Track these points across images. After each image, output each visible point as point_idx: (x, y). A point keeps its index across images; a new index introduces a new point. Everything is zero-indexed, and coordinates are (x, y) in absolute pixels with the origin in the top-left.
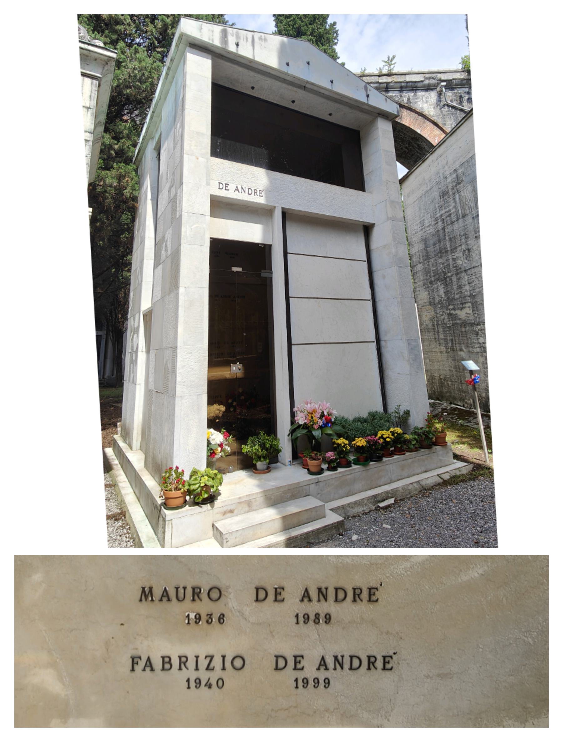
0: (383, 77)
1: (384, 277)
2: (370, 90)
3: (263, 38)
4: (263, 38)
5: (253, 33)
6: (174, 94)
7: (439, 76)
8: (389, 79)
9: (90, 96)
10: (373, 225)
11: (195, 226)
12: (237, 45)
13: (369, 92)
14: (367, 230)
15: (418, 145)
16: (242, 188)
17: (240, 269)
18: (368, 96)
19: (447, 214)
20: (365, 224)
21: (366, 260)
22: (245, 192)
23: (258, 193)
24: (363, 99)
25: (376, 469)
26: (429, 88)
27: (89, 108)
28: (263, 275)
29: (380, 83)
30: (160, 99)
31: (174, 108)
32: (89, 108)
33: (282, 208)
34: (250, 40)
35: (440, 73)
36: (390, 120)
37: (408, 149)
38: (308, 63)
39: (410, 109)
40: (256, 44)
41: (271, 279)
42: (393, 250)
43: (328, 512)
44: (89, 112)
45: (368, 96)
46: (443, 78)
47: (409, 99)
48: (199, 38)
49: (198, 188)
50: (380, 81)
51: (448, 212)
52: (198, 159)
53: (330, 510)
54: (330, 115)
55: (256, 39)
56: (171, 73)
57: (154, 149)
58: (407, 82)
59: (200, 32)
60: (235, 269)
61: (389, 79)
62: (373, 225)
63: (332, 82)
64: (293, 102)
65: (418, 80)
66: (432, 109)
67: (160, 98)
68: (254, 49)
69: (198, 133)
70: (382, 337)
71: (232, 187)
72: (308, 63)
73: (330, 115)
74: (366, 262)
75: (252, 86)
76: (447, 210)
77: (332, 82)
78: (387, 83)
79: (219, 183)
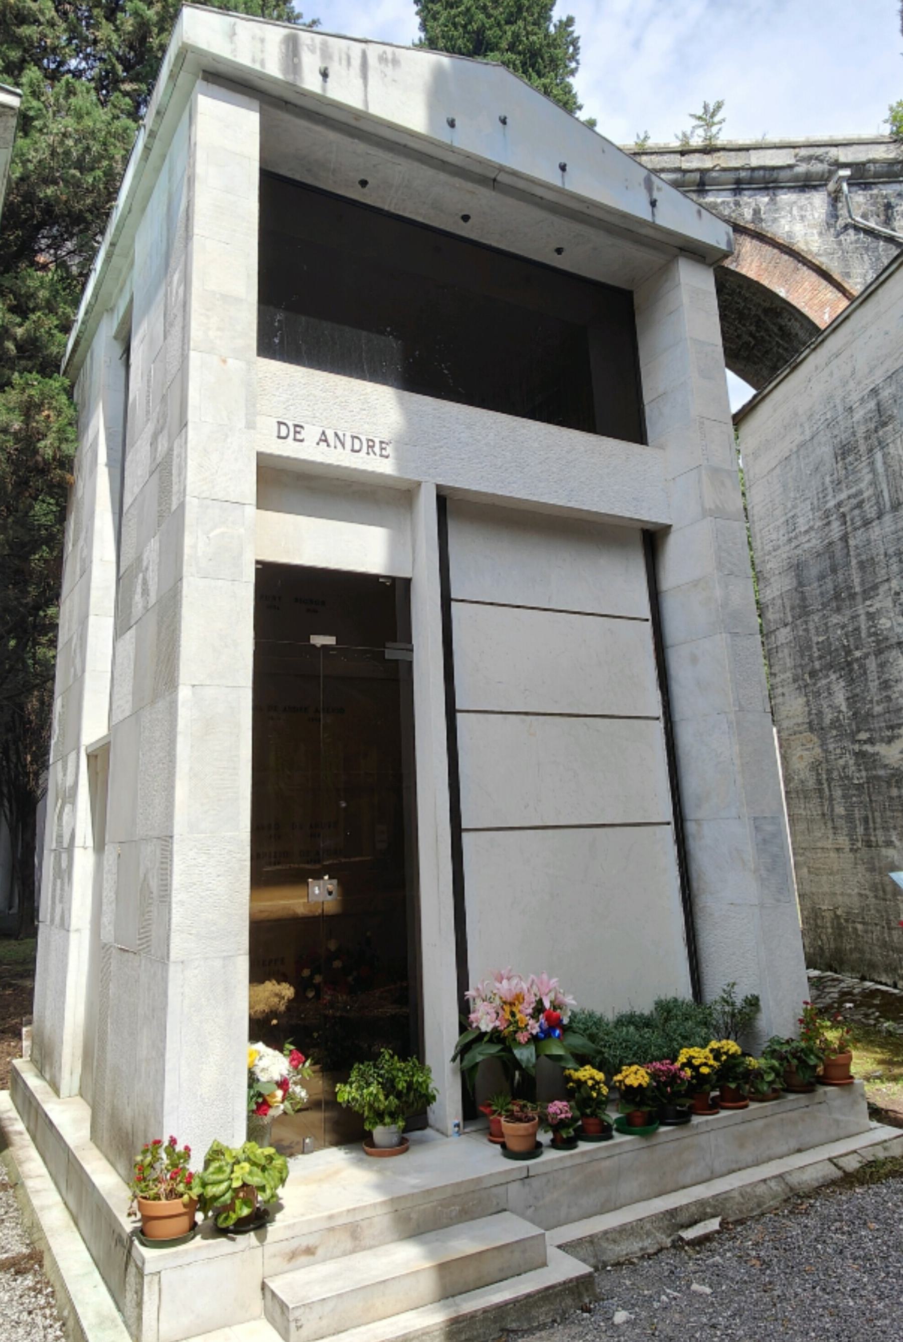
1: (694, 660)
2: (659, 189)
3: (390, 57)
4: (390, 57)
5: (363, 45)
6: (165, 199)
7: (833, 152)
10: (666, 529)
12: (325, 74)
13: (656, 195)
14: (652, 541)
15: (781, 328)
16: (336, 435)
18: (653, 204)
19: (854, 501)
21: (649, 617)
22: (343, 445)
23: (377, 449)
24: (642, 211)
26: (806, 184)
28: (389, 655)
29: (685, 172)
30: (129, 212)
33: (438, 487)
34: (356, 62)
35: (836, 146)
36: (710, 265)
38: (504, 121)
39: (760, 237)
40: (371, 74)
41: (410, 664)
42: (718, 593)
45: (653, 204)
46: (842, 159)
47: (756, 212)
48: (229, 56)
49: (227, 436)
50: (685, 166)
51: (855, 496)
52: (224, 361)
53: (559, 1247)
54: (559, 251)
59: (232, 42)
60: (318, 640)
61: (707, 162)
62: (666, 529)
63: (563, 168)
64: (466, 218)
70: (691, 812)
71: (311, 433)
72: (504, 121)
73: (559, 251)
74: (650, 623)
75: (362, 177)
77: (563, 168)
78: (703, 171)
79: (280, 423)
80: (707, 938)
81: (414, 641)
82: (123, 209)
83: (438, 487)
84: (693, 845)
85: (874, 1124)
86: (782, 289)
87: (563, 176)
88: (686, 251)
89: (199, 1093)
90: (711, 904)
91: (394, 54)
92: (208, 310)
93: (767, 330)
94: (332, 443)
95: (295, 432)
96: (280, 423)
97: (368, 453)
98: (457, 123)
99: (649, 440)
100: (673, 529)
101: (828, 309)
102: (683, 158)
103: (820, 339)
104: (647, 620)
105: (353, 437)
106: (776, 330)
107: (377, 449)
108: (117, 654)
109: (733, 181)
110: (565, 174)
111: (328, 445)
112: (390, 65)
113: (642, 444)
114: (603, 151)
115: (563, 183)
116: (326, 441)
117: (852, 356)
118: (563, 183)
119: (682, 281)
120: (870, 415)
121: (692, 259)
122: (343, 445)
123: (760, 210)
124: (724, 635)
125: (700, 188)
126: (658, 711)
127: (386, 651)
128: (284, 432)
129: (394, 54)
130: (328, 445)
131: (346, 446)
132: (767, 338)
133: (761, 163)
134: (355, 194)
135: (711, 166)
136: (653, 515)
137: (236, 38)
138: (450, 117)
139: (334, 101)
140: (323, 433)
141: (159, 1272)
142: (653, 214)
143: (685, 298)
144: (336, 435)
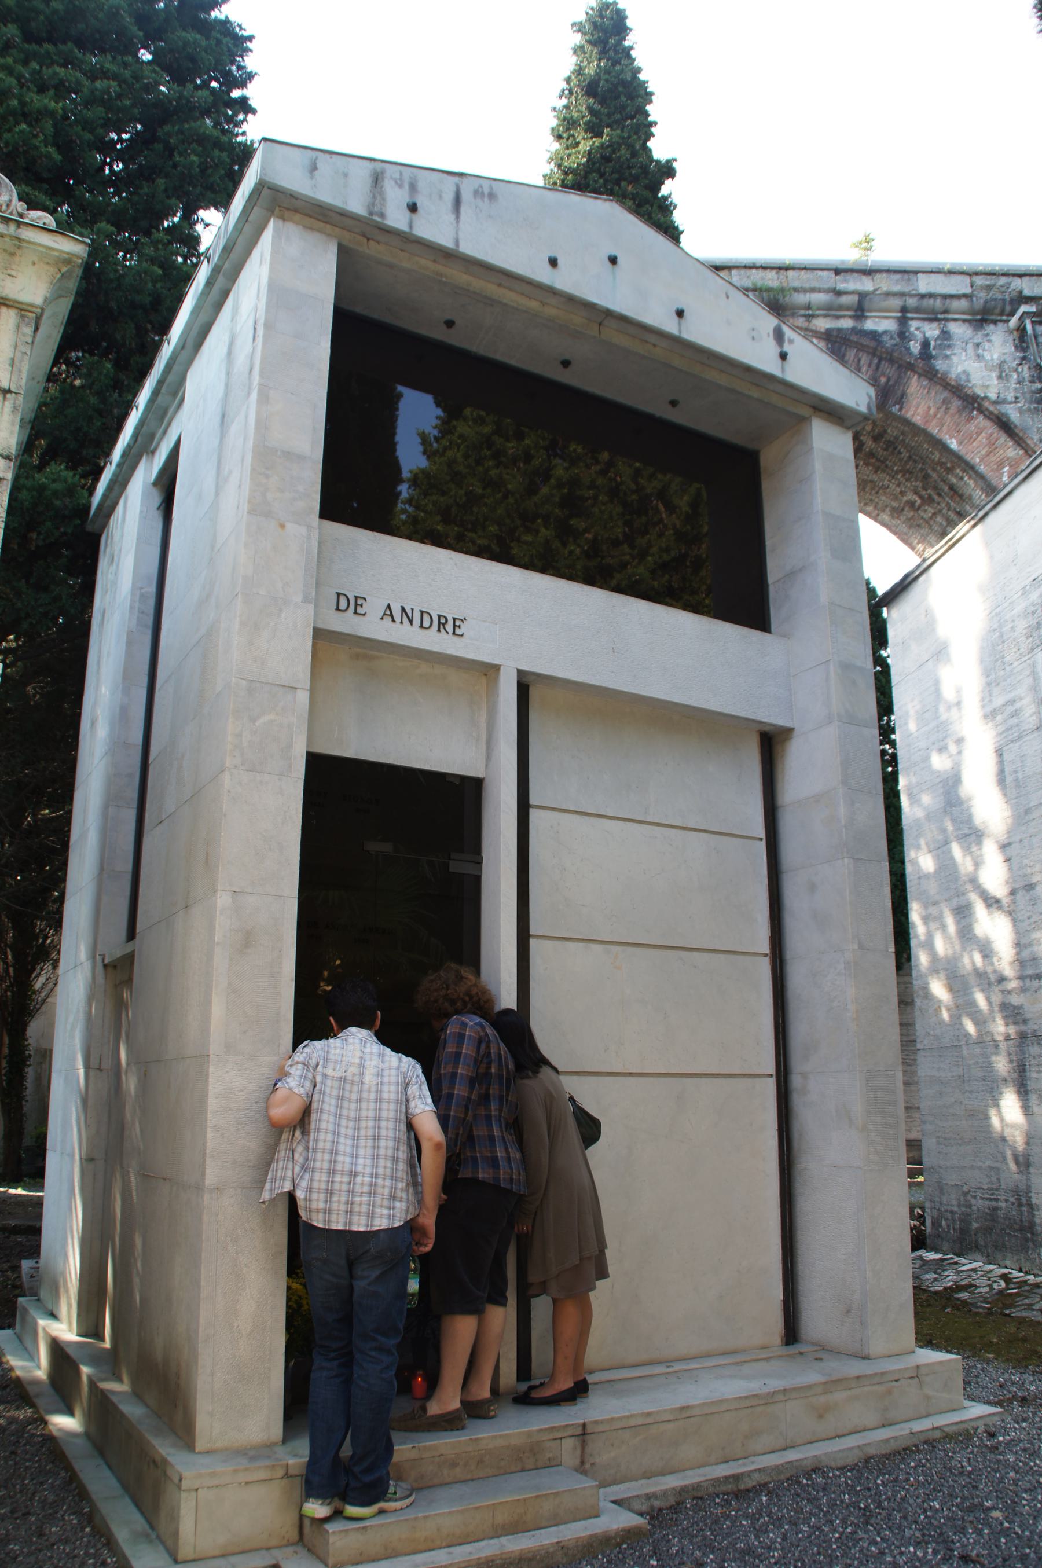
0: (848, 276)
1: (812, 888)
2: (791, 341)
3: (486, 191)
4: (486, 191)
5: (457, 179)
6: (226, 338)
7: (1017, 284)
8: (866, 285)
9: (13, 360)
10: (787, 733)
11: (266, 718)
12: (413, 208)
13: (787, 347)
14: (771, 743)
15: (952, 488)
16: (403, 609)
17: (387, 847)
18: (783, 356)
19: (1010, 709)
20: (766, 729)
21: (763, 835)
22: (411, 622)
23: (449, 627)
24: (769, 364)
25: (749, 1410)
26: (984, 317)
27: (9, 391)
28: (455, 867)
29: (839, 293)
30: (183, 347)
31: (223, 376)
32: (9, 391)
33: (519, 671)
34: (449, 197)
35: (1020, 276)
36: (848, 428)
37: (921, 497)
38: (613, 260)
39: (932, 376)
40: (463, 209)
41: (477, 880)
42: (842, 811)
43: (605, 1505)
44: (7, 403)
45: (783, 356)
46: (1027, 292)
47: (926, 344)
48: (313, 195)
49: (281, 610)
50: (841, 286)
51: (1012, 702)
52: (283, 526)
53: (614, 1502)
54: (674, 403)
55: (466, 195)
56: (221, 281)
57: (155, 484)
58: (923, 296)
59: (312, 178)
60: (374, 847)
61: (866, 285)
62: (787, 733)
63: (680, 313)
64: (566, 364)
65: (953, 292)
66: (996, 382)
67: (182, 345)
68: (458, 217)
69: (288, 455)
70: (797, 1064)
71: (374, 607)
72: (613, 260)
73: (674, 403)
74: (764, 843)
75: (448, 317)
76: (1009, 697)
77: (680, 313)
78: (862, 296)
79: (339, 594)
80: (806, 1205)
81: (484, 854)
82: (177, 344)
83: (519, 671)
84: (797, 1101)
85: (967, 1403)
86: (954, 440)
87: (680, 324)
88: (820, 411)
89: (236, 1325)
90: (812, 1166)
91: (491, 188)
92: (267, 469)
93: (935, 488)
94: (397, 618)
95: (356, 605)
96: (339, 594)
97: (439, 630)
98: (561, 262)
99: (774, 626)
100: (796, 733)
101: (1007, 469)
102: (838, 277)
103: (981, 514)
104: (761, 839)
105: (422, 612)
106: (946, 489)
107: (449, 627)
108: (566, 815)
109: (899, 308)
110: (683, 320)
111: (393, 621)
112: (486, 199)
113: (42, 1204)
114: (727, 297)
115: (680, 331)
116: (391, 615)
117: (1015, 538)
118: (680, 331)
119: (815, 445)
120: (1033, 609)
121: (827, 420)
122: (411, 622)
123: (929, 344)
124: (846, 860)
125: (859, 313)
126: (765, 947)
127: (451, 862)
128: (343, 604)
129: (491, 188)
130: (393, 621)
131: (414, 622)
132: (936, 497)
133: (932, 289)
134: (439, 334)
135: (871, 289)
136: (773, 717)
137: (316, 173)
138: (553, 255)
139: (422, 238)
140: (389, 606)
141: (197, 1490)
142: (783, 370)
143: (818, 466)
144: (403, 609)
